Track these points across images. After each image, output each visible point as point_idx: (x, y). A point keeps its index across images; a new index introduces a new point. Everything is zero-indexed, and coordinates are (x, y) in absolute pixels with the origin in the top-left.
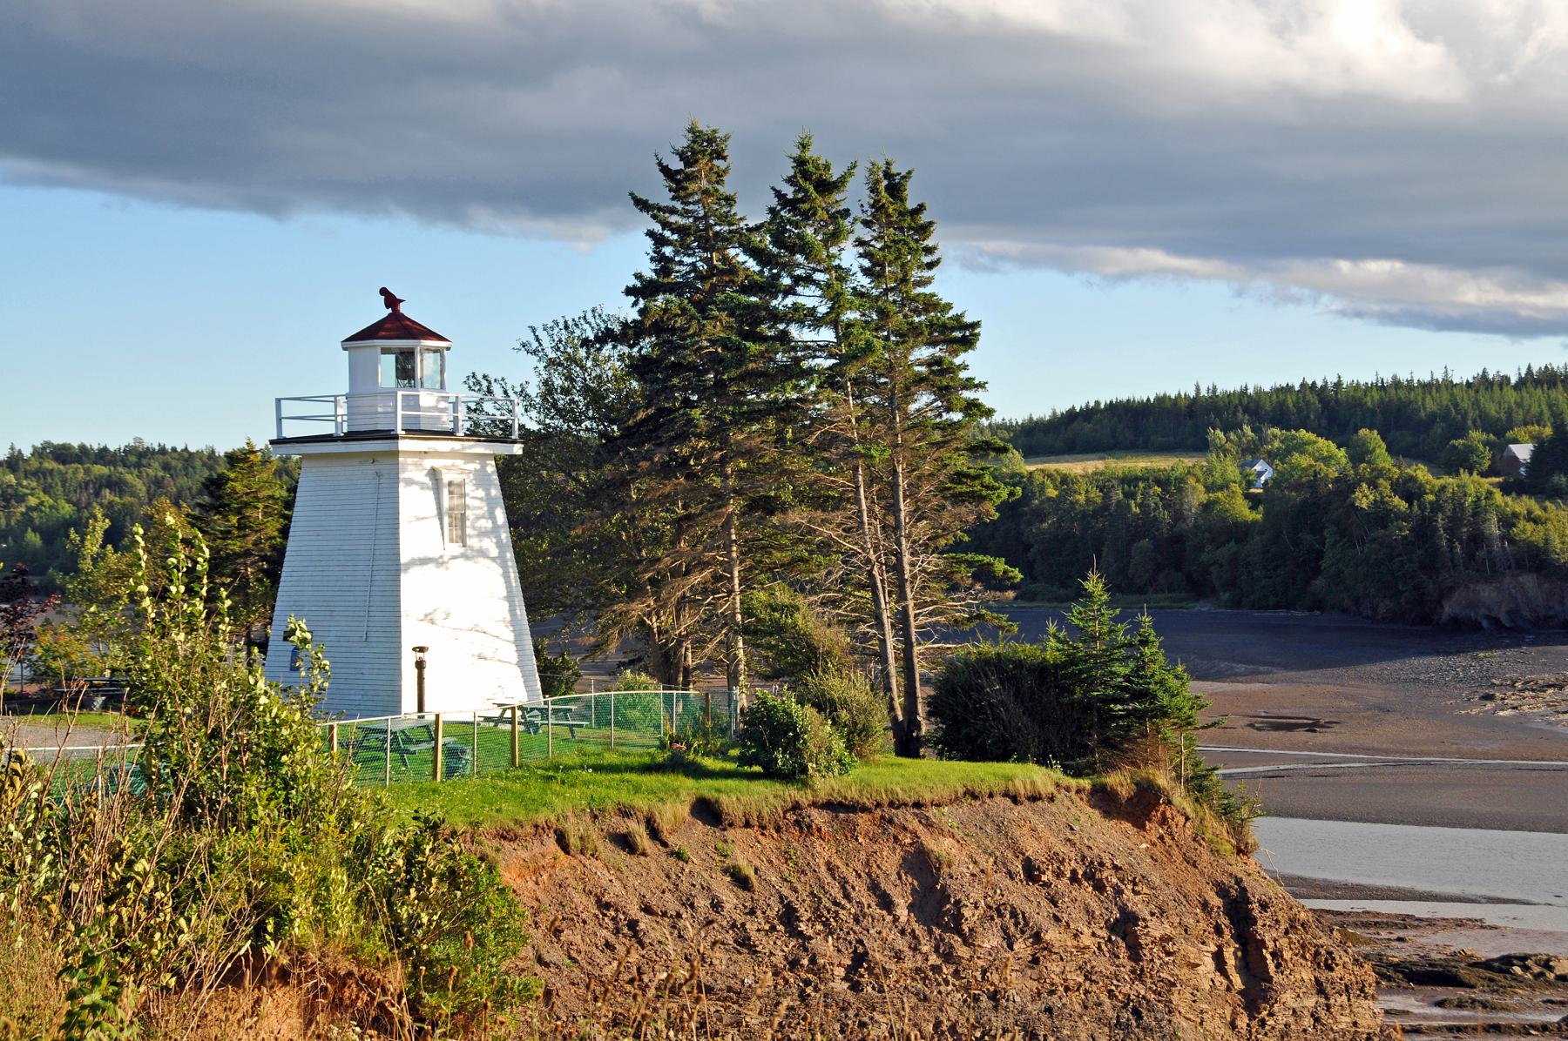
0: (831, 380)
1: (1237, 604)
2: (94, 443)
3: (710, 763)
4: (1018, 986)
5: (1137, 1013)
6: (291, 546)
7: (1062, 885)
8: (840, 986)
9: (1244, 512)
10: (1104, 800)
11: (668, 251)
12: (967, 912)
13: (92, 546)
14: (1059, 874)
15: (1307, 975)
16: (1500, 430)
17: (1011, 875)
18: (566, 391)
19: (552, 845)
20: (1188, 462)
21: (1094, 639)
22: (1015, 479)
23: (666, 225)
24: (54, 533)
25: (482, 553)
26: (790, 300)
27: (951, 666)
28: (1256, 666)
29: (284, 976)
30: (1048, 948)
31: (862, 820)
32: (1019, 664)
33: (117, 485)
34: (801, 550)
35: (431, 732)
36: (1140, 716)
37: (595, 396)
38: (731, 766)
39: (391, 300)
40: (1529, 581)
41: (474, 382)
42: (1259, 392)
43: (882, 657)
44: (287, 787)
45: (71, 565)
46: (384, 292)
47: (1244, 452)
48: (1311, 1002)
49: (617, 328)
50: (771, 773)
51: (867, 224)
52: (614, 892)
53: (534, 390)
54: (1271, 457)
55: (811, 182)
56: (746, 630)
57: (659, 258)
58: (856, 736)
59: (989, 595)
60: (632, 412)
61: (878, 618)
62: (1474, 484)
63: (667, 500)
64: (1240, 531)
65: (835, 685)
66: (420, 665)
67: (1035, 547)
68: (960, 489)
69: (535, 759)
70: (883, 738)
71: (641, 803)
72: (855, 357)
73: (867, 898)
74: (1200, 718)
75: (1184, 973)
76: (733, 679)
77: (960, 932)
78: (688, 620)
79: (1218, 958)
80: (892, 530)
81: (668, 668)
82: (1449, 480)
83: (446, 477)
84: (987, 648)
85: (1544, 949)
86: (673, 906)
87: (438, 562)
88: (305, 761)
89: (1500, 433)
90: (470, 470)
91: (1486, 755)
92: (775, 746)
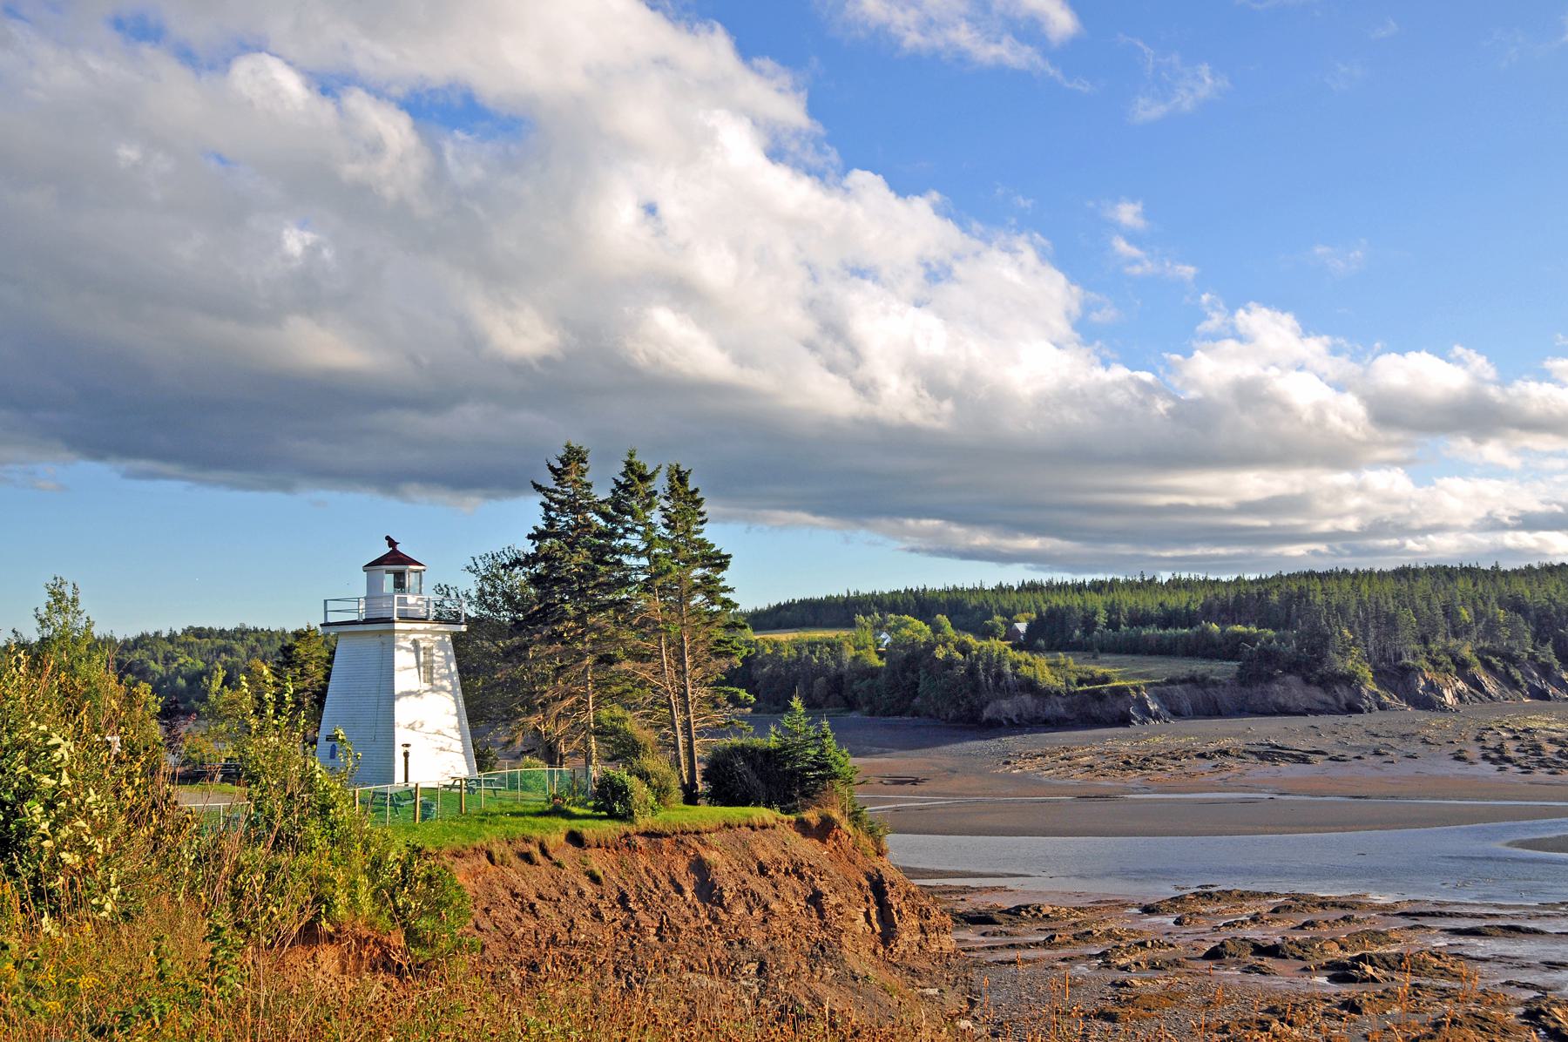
0: (647, 587)
1: (872, 713)
2: (217, 627)
3: (576, 810)
4: (756, 937)
5: (822, 948)
6: (331, 684)
7: (780, 876)
8: (653, 939)
9: (875, 661)
10: (803, 827)
11: (553, 514)
12: (726, 894)
13: (216, 686)
14: (778, 871)
15: (915, 923)
16: (1009, 615)
17: (751, 872)
18: (492, 594)
19: (484, 860)
20: (843, 633)
21: (797, 734)
22: (748, 644)
23: (551, 499)
24: (195, 678)
25: (443, 689)
26: (622, 542)
27: (716, 752)
28: (883, 747)
29: (330, 938)
30: (773, 913)
31: (665, 842)
32: (754, 750)
33: (229, 651)
34: (628, 686)
35: (412, 794)
36: (822, 778)
37: (509, 598)
38: (589, 812)
39: (392, 543)
40: (1027, 698)
41: (439, 589)
42: (882, 594)
43: (676, 747)
44: (332, 828)
45: (203, 698)
46: (388, 538)
47: (875, 627)
48: (917, 938)
49: (522, 558)
50: (612, 816)
51: (667, 498)
52: (521, 886)
53: (473, 594)
54: (890, 630)
55: (635, 475)
56: (596, 733)
57: (548, 518)
58: (661, 793)
59: (736, 710)
60: (531, 607)
61: (673, 724)
62: (997, 645)
63: (550, 657)
64: (873, 673)
65: (650, 763)
66: (406, 755)
67: (766, 686)
68: (720, 650)
69: (473, 809)
70: (677, 794)
71: (536, 834)
72: (660, 575)
73: (669, 888)
74: (856, 779)
75: (848, 925)
76: (588, 761)
77: (721, 905)
78: (562, 727)
79: (867, 915)
80: (681, 673)
81: (551, 755)
82: (985, 643)
83: (422, 645)
84: (736, 741)
85: (1036, 901)
86: (555, 894)
87: (417, 694)
88: (343, 813)
89: (1009, 617)
90: (435, 639)
91: (1007, 795)
92: (615, 799)
